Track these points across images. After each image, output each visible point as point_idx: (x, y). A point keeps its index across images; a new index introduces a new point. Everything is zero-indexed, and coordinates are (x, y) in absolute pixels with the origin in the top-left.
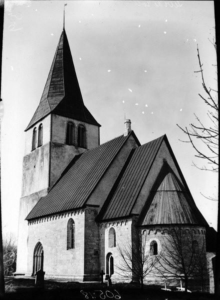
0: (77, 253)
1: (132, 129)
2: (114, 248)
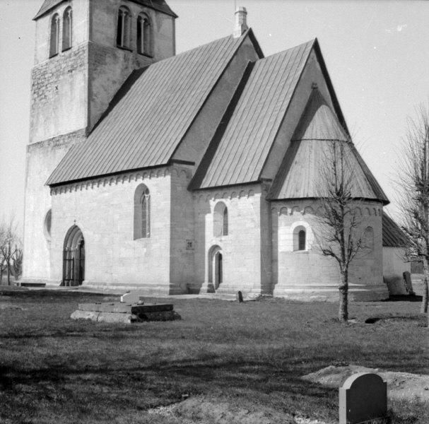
0: (155, 246)
1: (250, 24)
2: (224, 238)
